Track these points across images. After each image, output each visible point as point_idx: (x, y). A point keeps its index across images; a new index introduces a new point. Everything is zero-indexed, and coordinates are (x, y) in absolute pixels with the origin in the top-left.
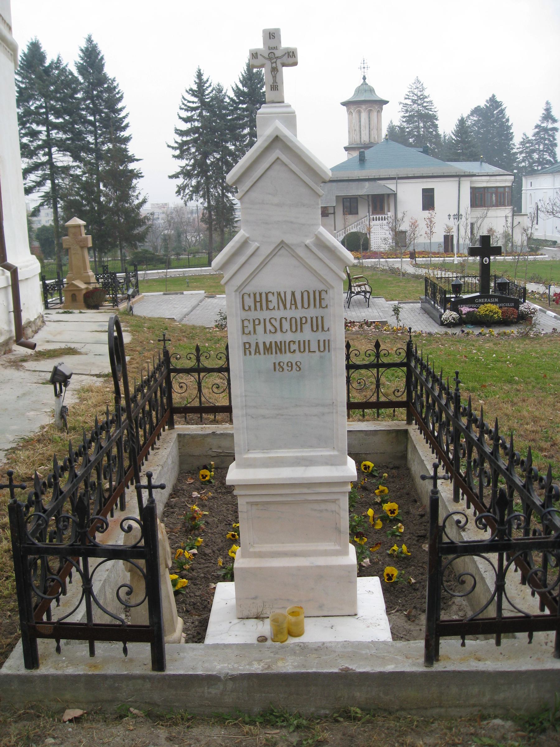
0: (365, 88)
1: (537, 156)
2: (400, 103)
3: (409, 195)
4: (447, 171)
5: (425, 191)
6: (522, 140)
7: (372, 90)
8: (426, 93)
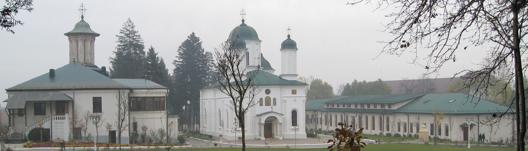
0: (83, 24)
2: (117, 36)
3: (83, 103)
4: (111, 85)
5: (95, 99)
7: (87, 26)
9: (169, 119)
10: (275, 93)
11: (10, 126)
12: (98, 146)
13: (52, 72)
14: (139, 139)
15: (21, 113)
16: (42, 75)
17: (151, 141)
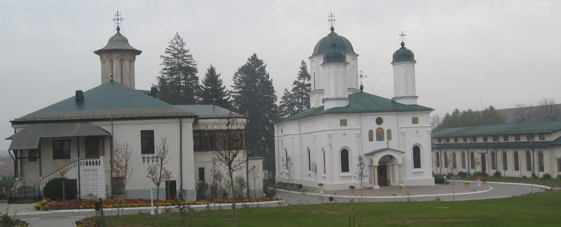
0: (119, 38)
1: (297, 109)
2: (162, 56)
3: (127, 136)
6: (284, 95)
7: (125, 40)
8: (186, 48)
9: (249, 161)
10: (390, 122)
11: (16, 176)
12: (157, 206)
13: (79, 94)
14: (208, 192)
15: (34, 155)
16: (65, 100)
17: (225, 195)
